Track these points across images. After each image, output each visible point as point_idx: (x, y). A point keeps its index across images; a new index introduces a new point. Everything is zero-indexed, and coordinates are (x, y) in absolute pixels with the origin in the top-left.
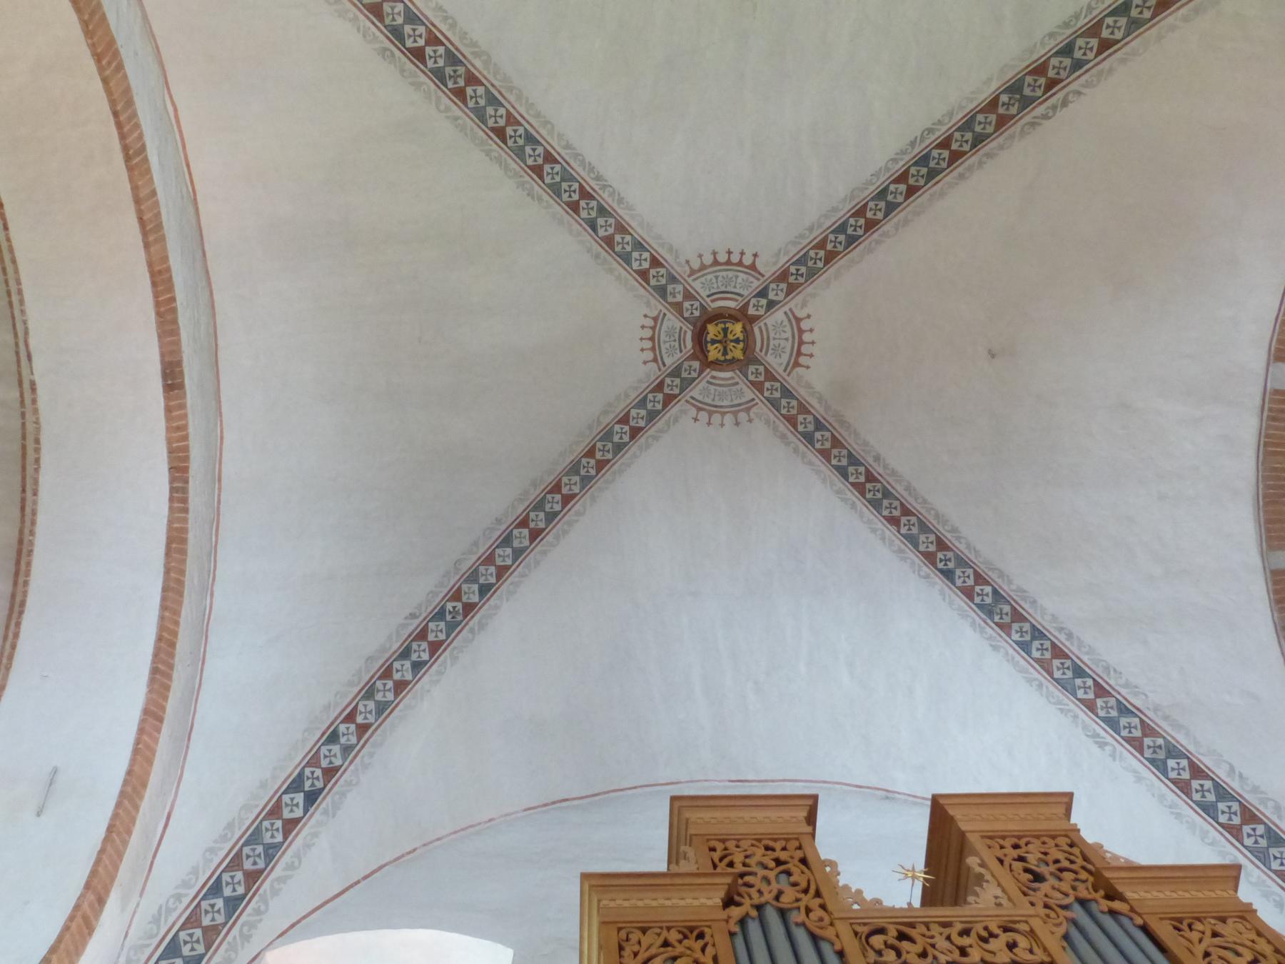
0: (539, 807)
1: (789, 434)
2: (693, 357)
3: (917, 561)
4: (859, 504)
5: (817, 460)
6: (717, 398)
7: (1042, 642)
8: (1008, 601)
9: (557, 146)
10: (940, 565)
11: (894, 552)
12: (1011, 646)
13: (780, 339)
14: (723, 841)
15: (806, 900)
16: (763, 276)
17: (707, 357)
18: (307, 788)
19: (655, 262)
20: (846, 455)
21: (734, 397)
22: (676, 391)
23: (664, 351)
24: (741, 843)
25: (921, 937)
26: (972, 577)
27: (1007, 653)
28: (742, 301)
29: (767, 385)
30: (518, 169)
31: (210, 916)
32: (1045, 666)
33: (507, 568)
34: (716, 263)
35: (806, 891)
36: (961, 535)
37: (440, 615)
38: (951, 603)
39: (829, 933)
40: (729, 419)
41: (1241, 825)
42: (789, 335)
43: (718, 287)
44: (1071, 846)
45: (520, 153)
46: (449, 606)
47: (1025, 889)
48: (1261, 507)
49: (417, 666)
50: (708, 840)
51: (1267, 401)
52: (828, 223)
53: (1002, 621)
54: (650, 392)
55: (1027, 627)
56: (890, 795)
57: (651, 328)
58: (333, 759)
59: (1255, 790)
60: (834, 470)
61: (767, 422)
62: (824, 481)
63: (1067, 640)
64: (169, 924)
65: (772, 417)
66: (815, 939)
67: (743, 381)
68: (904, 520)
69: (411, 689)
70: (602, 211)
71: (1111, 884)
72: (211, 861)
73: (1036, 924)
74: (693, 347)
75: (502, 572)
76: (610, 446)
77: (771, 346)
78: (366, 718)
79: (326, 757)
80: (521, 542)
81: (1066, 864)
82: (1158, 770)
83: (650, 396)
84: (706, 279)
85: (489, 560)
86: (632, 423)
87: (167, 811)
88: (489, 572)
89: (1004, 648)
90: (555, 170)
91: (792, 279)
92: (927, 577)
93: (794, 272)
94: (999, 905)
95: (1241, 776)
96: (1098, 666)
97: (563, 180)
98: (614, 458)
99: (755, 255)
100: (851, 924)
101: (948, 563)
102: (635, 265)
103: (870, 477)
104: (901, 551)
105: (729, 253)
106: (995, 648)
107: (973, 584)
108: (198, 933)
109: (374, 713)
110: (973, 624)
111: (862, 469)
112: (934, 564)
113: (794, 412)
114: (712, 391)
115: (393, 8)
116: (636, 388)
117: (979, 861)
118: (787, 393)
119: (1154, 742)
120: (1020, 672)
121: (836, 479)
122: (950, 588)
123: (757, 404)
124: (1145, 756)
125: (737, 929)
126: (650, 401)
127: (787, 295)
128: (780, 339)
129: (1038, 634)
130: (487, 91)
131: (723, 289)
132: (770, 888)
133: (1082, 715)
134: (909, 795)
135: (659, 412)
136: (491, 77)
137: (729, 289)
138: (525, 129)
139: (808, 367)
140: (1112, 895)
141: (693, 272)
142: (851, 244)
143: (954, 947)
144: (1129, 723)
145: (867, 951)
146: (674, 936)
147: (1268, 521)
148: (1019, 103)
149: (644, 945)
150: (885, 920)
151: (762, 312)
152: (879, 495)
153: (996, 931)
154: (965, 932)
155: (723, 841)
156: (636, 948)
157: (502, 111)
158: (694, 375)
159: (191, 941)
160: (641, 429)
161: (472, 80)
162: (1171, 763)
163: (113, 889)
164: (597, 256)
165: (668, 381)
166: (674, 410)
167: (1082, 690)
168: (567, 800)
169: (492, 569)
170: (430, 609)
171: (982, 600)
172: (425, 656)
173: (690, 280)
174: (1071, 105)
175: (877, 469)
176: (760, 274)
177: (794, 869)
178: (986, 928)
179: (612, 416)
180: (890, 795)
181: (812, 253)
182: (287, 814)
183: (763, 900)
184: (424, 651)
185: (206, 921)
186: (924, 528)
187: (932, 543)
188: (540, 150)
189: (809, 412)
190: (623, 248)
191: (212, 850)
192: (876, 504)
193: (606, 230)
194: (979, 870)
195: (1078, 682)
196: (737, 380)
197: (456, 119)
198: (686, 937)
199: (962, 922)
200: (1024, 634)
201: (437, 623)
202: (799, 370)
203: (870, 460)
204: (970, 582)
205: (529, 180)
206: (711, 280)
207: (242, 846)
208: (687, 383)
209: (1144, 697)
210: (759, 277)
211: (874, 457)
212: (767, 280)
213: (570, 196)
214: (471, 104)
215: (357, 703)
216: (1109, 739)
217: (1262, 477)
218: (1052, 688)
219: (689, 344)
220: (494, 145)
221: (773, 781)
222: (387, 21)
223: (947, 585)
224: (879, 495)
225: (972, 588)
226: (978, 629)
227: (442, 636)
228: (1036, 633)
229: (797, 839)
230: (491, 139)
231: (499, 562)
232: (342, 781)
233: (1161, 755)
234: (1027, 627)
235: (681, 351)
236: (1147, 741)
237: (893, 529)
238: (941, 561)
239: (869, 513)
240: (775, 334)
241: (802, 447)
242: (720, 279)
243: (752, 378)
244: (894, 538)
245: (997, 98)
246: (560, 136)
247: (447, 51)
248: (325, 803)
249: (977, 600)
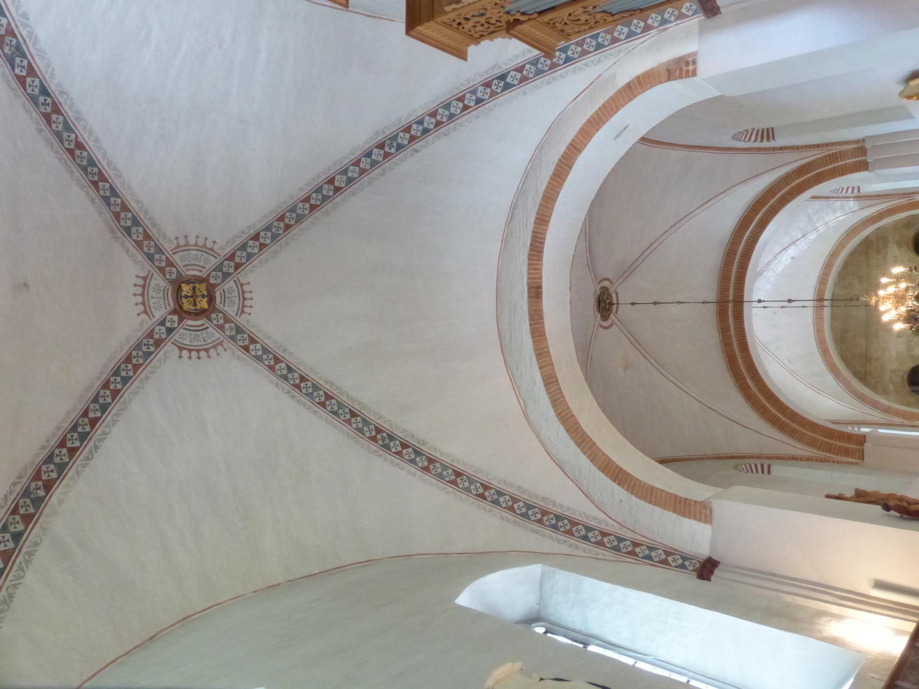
0: (385, 19)
2: (214, 286)
3: (66, 108)
4: (105, 164)
5: (132, 204)
6: (199, 256)
9: (320, 411)
12: (11, 14)
13: (156, 298)
16: (172, 343)
17: (183, 283)
18: (503, 82)
19: (246, 348)
21: (187, 256)
22: (226, 263)
23: (236, 291)
27: (17, 9)
28: (183, 325)
29: (163, 264)
30: (341, 397)
31: (576, 50)
33: (353, 165)
34: (207, 350)
37: (400, 147)
40: (192, 241)
42: (152, 301)
43: (202, 334)
45: (340, 405)
46: (393, 151)
49: (420, 122)
52: (136, 383)
54: (244, 263)
57: (246, 306)
58: (483, 90)
60: (120, 194)
61: (164, 236)
64: (595, 57)
65: (161, 240)
67: (180, 268)
69: (429, 111)
70: (285, 378)
72: (564, 72)
74: (215, 292)
75: (357, 163)
76: (274, 230)
77: (162, 292)
78: (457, 104)
79: (487, 93)
80: (341, 178)
83: (244, 260)
84: (211, 339)
85: (363, 172)
86: (257, 243)
87: (574, 102)
88: (364, 164)
89: (18, 14)
90: (317, 398)
91: (151, 341)
92: (62, 93)
93: (150, 347)
97: (312, 394)
98: (273, 222)
99: (180, 357)
102: (259, 346)
104: (79, 119)
105: (199, 358)
106: (25, 16)
108: (585, 47)
109: (452, 105)
110: (36, 42)
112: (54, 103)
113: (146, 243)
114: (202, 261)
115: (423, 464)
116: (255, 266)
118: (150, 257)
121: (119, 186)
122: (44, 78)
123: (171, 251)
126: (244, 257)
127: (153, 330)
128: (156, 298)
130: (364, 435)
131: (199, 333)
135: (239, 249)
136: (364, 442)
137: (195, 333)
138: (340, 419)
139: (137, 276)
141: (221, 344)
142: (117, 369)
148: (30, 491)
151: (169, 317)
157: (354, 426)
158: (214, 274)
159: (590, 45)
160: (252, 239)
161: (373, 439)
163: (620, 87)
164: (284, 351)
165: (231, 270)
166: (228, 250)
168: (368, 16)
169: (362, 165)
170: (405, 152)
172: (415, 126)
173: (222, 338)
174: (2, 497)
176: (175, 345)
179: (271, 249)
181: (141, 361)
182: (519, 75)
184: (414, 129)
185: (579, 49)
188: (329, 408)
189: (135, 241)
190: (268, 357)
191: (562, 76)
192: (92, 162)
193: (280, 367)
196: (184, 269)
197: (380, 418)
201: (402, 143)
202: (144, 275)
205: (334, 392)
206: (208, 339)
207: (547, 71)
208: (219, 268)
210: (175, 342)
212: (169, 340)
213: (306, 385)
214: (372, 427)
215: (460, 113)
219: (218, 295)
220: (356, 407)
222: (424, 457)
227: (401, 134)
230: (358, 410)
231: (357, 169)
232: (483, 78)
235: (224, 290)
237: (80, 139)
239: (98, 155)
240: (160, 301)
241: (142, 215)
242: (202, 340)
243: (174, 270)
244: (82, 132)
245: (47, 491)
246: (320, 417)
247: (390, 450)
248: (497, 72)
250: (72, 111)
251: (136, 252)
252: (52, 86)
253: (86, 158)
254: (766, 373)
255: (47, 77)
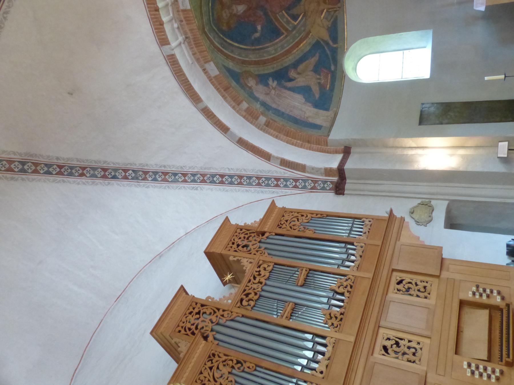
1: (14, 176)
3: (101, 181)
4: (65, 179)
5: (35, 176)
7: (158, 174)
8: (140, 171)
10: (110, 176)
11: (91, 185)
12: (151, 183)
14: (178, 326)
15: (218, 313)
20: (44, 166)
24: (183, 320)
25: (249, 290)
26: (122, 172)
27: (152, 186)
32: (165, 180)
35: (215, 312)
36: (193, 190)
38: (124, 185)
39: (234, 315)
41: (241, 181)
44: (241, 230)
47: (249, 252)
48: (186, 94)
50: (175, 331)
51: (167, 60)
53: (142, 178)
55: (151, 174)
56: (160, 255)
59: (237, 170)
62: (45, 181)
63: (165, 168)
66: (232, 320)
68: (85, 172)
71: (260, 231)
73: (261, 258)
81: (247, 236)
82: (213, 183)
92: (109, 183)
94: (251, 263)
95: (232, 169)
96: (179, 169)
100: (235, 307)
101: (111, 174)
103: (60, 167)
104: (93, 183)
106: (148, 187)
107: (125, 174)
110: (135, 186)
111: (55, 166)
112: (107, 178)
117: (233, 257)
119: (207, 177)
120: (160, 188)
121: (49, 177)
124: (208, 182)
125: (217, 342)
129: (155, 173)
132: (207, 322)
133: (185, 185)
134: (165, 250)
140: (263, 234)
143: (258, 284)
144: (198, 177)
145: (247, 308)
146: (209, 364)
147: (191, 96)
149: (207, 375)
150: (239, 297)
152: (69, 170)
153: (258, 270)
154: (255, 278)
155: (178, 326)
156: (207, 379)
162: (215, 179)
167: (180, 179)
171: (132, 176)
175: (61, 162)
177: (204, 310)
178: (256, 272)
180: (160, 255)
183: (210, 327)
186: (94, 169)
187: (101, 172)
189: (14, 161)
192: (71, 174)
194: (235, 259)
195: (177, 177)
198: (212, 360)
199: (251, 276)
200: (152, 176)
203: (56, 161)
204: (123, 174)
209: (196, 168)
211: (56, 159)
216: (197, 186)
217: (181, 84)
218: (172, 185)
221: (127, 287)
223: (117, 181)
224: (69, 170)
225: (125, 175)
226: (138, 186)
228: (155, 173)
229: (193, 302)
233: (211, 179)
234: (151, 174)
236: (206, 178)
238: (109, 175)
239: (71, 179)
241: (24, 176)
244: (87, 180)
249: (130, 177)
250: (99, 182)
251: (9, 157)
252: (114, 182)
253: (74, 173)
254: (345, 213)
255: (119, 182)
